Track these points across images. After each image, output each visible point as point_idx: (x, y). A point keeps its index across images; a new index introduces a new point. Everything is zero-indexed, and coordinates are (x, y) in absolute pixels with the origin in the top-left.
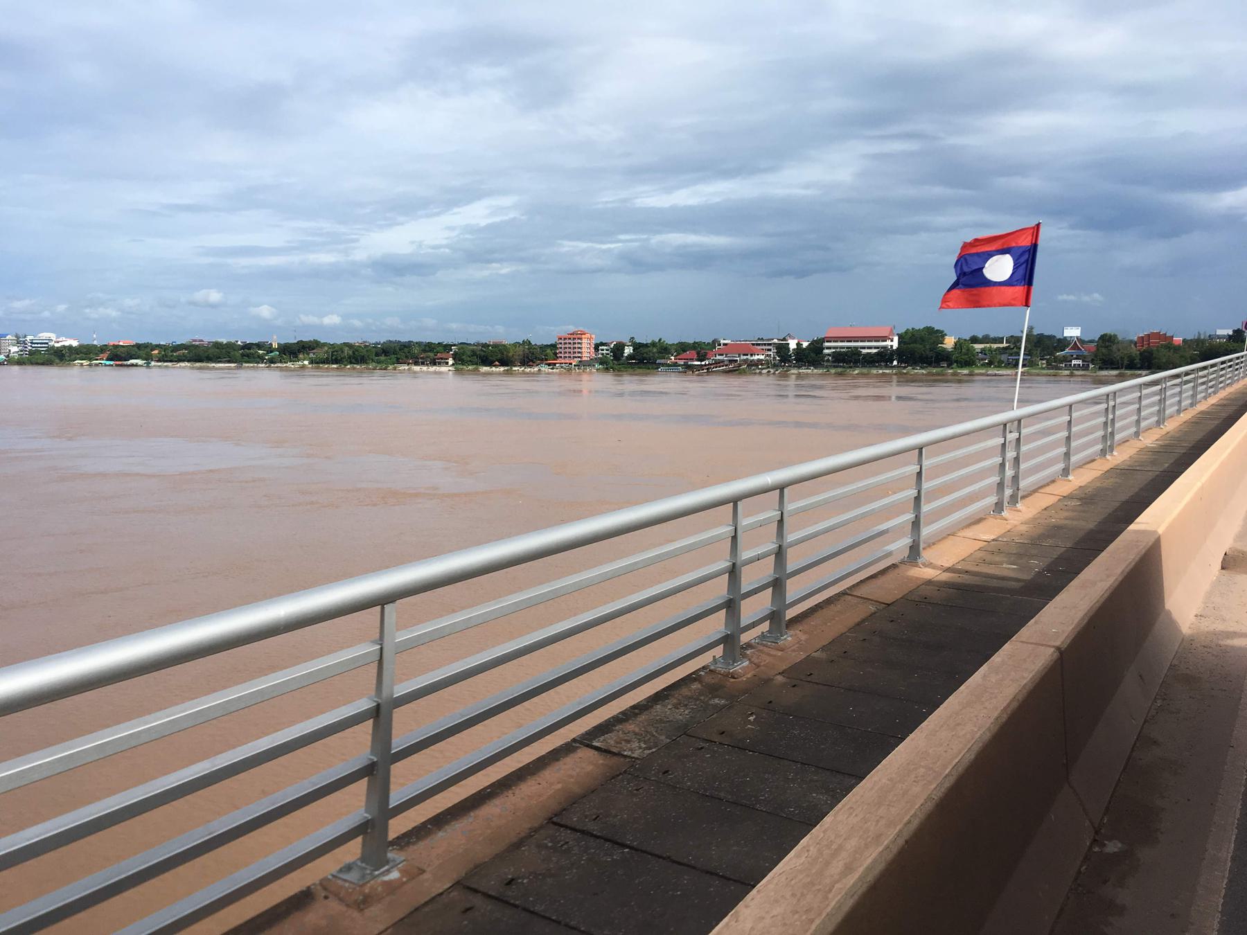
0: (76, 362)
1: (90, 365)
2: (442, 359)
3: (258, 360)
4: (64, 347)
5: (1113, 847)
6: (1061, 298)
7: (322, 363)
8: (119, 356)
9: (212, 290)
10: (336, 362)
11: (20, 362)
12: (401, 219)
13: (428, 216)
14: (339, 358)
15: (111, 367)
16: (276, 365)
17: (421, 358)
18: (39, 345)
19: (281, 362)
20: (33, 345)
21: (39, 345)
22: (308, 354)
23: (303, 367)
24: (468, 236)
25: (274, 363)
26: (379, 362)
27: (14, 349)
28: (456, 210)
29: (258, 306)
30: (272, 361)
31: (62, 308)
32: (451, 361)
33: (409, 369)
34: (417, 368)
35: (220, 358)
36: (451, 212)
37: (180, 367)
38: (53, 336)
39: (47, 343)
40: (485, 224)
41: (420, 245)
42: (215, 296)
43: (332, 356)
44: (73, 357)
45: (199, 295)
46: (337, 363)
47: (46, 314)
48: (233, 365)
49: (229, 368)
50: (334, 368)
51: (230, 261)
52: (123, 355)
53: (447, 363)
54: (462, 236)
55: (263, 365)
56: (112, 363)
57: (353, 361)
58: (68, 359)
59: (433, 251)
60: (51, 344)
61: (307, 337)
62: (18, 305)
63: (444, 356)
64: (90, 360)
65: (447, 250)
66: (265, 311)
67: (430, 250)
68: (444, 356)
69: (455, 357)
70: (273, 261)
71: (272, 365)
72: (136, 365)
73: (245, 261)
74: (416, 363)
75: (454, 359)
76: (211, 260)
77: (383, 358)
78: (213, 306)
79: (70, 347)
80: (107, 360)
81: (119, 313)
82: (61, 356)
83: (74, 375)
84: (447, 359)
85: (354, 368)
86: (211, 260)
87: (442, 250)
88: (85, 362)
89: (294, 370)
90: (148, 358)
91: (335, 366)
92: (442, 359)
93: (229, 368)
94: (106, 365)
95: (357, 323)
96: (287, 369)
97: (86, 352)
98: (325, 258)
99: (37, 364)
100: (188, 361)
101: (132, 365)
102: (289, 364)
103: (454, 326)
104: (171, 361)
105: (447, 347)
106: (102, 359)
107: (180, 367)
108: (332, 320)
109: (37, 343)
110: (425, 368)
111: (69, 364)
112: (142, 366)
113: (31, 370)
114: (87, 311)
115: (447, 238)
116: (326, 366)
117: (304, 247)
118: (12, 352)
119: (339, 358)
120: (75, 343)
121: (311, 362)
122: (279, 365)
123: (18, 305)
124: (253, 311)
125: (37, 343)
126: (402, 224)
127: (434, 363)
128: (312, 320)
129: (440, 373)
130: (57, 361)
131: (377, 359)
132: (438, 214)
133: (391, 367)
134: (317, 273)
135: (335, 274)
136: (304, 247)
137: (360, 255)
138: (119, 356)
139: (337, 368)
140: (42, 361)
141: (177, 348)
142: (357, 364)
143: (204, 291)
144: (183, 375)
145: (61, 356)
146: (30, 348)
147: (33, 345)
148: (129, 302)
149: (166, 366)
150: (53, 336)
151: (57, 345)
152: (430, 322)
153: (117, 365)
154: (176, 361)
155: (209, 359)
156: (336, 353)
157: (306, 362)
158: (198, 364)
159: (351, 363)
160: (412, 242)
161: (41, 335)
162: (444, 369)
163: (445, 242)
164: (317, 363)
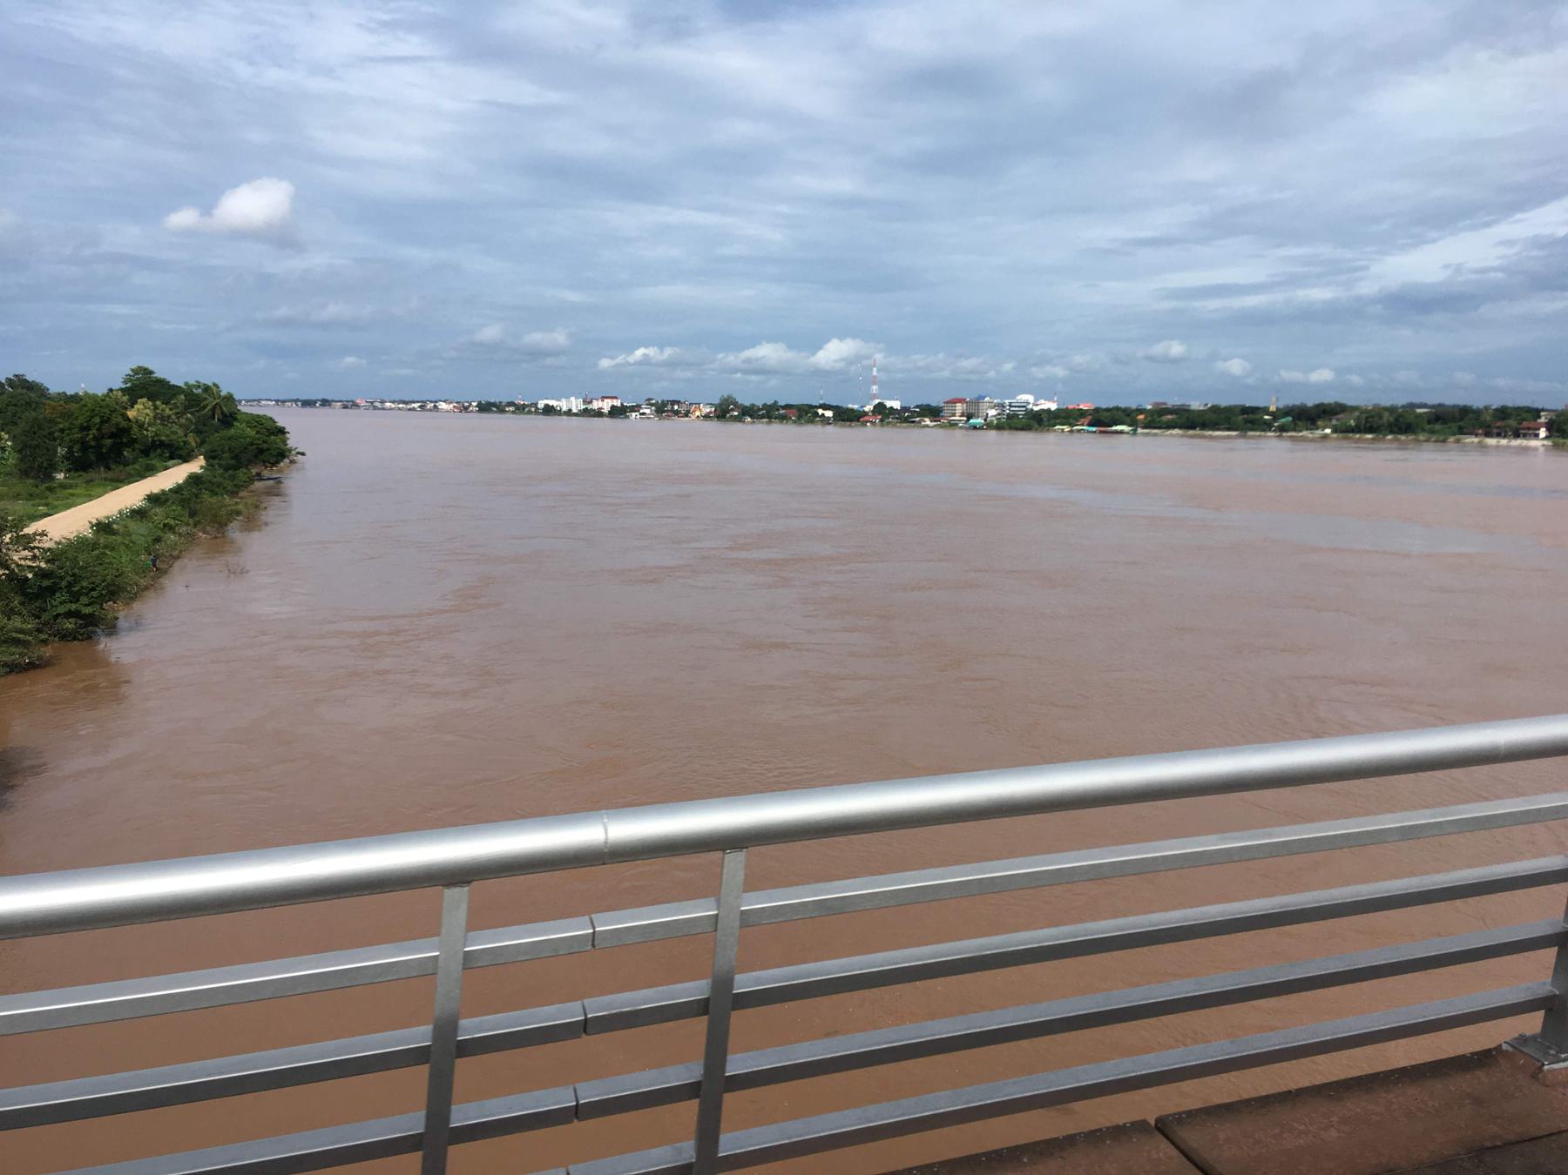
0: (1056, 427)
1: (1071, 431)
2: (1529, 429)
3: (1265, 427)
4: (1043, 410)
5: (1253, 1103)
6: (605, 363)
7: (1350, 432)
8: (1104, 420)
9: (1173, 343)
10: (1370, 430)
11: (999, 427)
12: (1433, 234)
13: (1473, 228)
14: (1375, 426)
15: (1093, 435)
16: (1289, 434)
17: (1498, 428)
18: (1017, 409)
19: (1294, 430)
20: (1012, 409)
21: (1017, 409)
22: (1330, 420)
23: (1325, 437)
24: (1535, 253)
25: (1286, 431)
26: (1432, 432)
27: (992, 412)
28: (1519, 216)
29: (1226, 359)
30: (1282, 429)
31: (1008, 367)
32: (1543, 433)
33: (1480, 442)
34: (1492, 441)
35: (1217, 424)
36: (1511, 220)
37: (1171, 435)
38: (1031, 398)
39: (1024, 407)
40: (1563, 234)
41: (1458, 269)
42: (1176, 349)
43: (1366, 422)
44: (1052, 422)
45: (1158, 349)
46: (1370, 432)
47: (992, 374)
48: (1234, 433)
49: (1228, 437)
50: (1367, 439)
51: (1197, 304)
52: (1107, 421)
53: (1537, 436)
54: (1524, 254)
55: (1272, 434)
56: (1094, 429)
57: (1396, 429)
58: (1047, 423)
59: (1479, 276)
60: (1030, 407)
61: (1329, 399)
62: (966, 364)
63: (1532, 425)
64: (1072, 425)
65: (1500, 275)
66: (1236, 366)
67: (1473, 276)
68: (1532, 425)
69: (1550, 426)
70: (1251, 301)
71: (1284, 434)
72: (1121, 432)
73: (1214, 304)
74: (1488, 435)
75: (1548, 429)
76: (1174, 304)
77: (1438, 427)
78: (1175, 361)
79: (1049, 410)
80: (1089, 425)
81: (1067, 372)
82: (1038, 421)
83: (1054, 441)
84: (1539, 429)
85: (1398, 440)
86: (1174, 304)
87: (1493, 275)
88: (1066, 428)
89: (1312, 440)
90: (1133, 423)
91: (1370, 436)
92: (1529, 429)
93: (1228, 437)
94: (1088, 432)
95: (1356, 379)
96: (1304, 439)
97: (1065, 417)
98: (1319, 294)
99: (1017, 429)
100: (1180, 428)
101: (1117, 432)
102: (1305, 433)
103: (1501, 382)
104: (1159, 428)
105: (1536, 413)
106: (1082, 425)
107: (1171, 435)
108: (1323, 375)
109: (1016, 407)
110: (1504, 442)
111: (1048, 430)
112: (1127, 433)
113: (1006, 434)
114: (1034, 369)
115: (1499, 258)
116: (1358, 436)
117: (1293, 281)
118: (989, 415)
119: (1375, 426)
120: (1053, 407)
121: (1335, 430)
122: (1293, 434)
123: (966, 364)
124: (1221, 366)
125: (1016, 407)
126: (1434, 241)
127: (1517, 435)
128: (1295, 376)
129: (1526, 449)
130: (1036, 426)
131: (1430, 429)
132: (1488, 225)
133: (1452, 439)
134: (1308, 315)
135: (1331, 314)
136: (1293, 281)
137: (1367, 288)
138: (1104, 420)
139: (1373, 439)
140: (1020, 426)
141: (1378, 412)
142: (1401, 434)
143: (1165, 343)
144: (1172, 446)
145: (1038, 421)
146: (1008, 411)
147: (1012, 409)
148: (1079, 359)
149: (1155, 435)
150: (1031, 398)
151: (1036, 408)
152: (1465, 377)
153: (1101, 432)
154: (1165, 428)
155: (1204, 426)
156: (1370, 420)
157: (1328, 431)
158: (1191, 432)
159: (1392, 432)
160: (1447, 266)
161: (1019, 397)
162: (1533, 443)
163: (1495, 263)
164: (1342, 432)
